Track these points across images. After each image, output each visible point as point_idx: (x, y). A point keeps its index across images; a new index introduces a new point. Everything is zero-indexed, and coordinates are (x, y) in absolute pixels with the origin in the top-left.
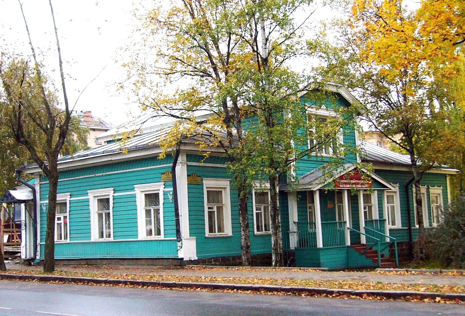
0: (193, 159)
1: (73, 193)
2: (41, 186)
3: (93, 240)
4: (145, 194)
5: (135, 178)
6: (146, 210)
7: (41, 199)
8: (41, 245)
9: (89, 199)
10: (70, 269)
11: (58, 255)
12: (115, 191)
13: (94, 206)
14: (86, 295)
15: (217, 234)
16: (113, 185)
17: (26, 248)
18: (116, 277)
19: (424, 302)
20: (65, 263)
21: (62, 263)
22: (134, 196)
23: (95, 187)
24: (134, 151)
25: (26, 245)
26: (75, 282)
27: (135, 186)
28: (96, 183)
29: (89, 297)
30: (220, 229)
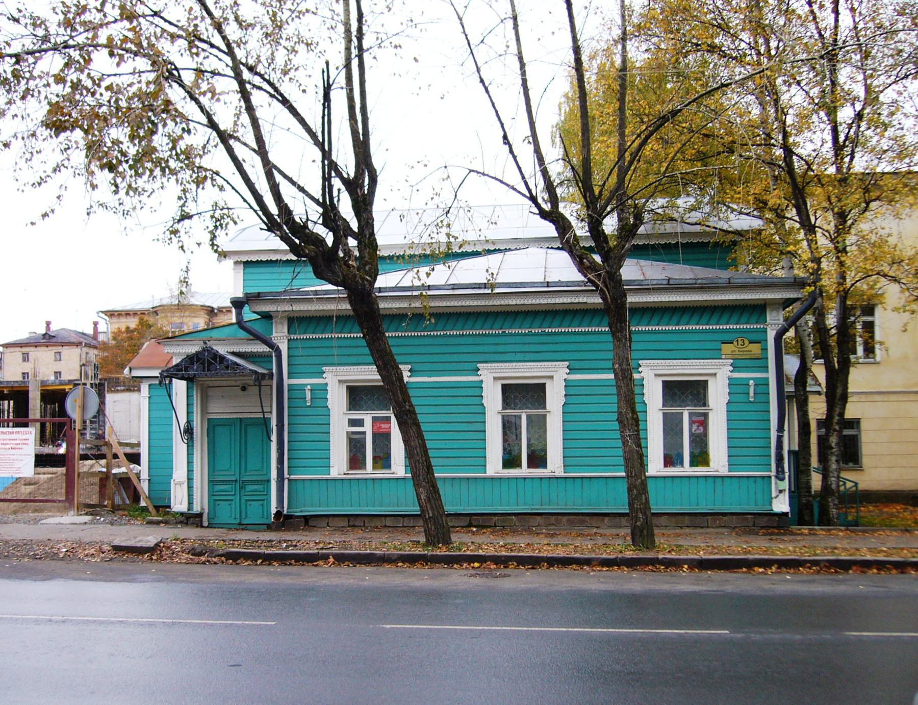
0: (686, 320)
1: (417, 367)
2: (294, 344)
3: (334, 473)
4: (664, 382)
5: (517, 348)
6: (664, 414)
7: (290, 375)
8: (289, 480)
9: (327, 384)
10: (384, 537)
11: (312, 505)
12: (571, 369)
13: (493, 399)
14: (35, 580)
15: (686, 469)
16: (566, 356)
17: (190, 488)
18: (537, 551)
19: (848, 573)
20: (389, 522)
21: (378, 523)
22: (479, 386)
23: (504, 357)
24: (663, 289)
25: (190, 479)
26: (235, 560)
27: (640, 362)
28: (501, 349)
29: (38, 583)
30: (700, 457)
